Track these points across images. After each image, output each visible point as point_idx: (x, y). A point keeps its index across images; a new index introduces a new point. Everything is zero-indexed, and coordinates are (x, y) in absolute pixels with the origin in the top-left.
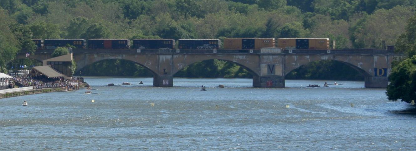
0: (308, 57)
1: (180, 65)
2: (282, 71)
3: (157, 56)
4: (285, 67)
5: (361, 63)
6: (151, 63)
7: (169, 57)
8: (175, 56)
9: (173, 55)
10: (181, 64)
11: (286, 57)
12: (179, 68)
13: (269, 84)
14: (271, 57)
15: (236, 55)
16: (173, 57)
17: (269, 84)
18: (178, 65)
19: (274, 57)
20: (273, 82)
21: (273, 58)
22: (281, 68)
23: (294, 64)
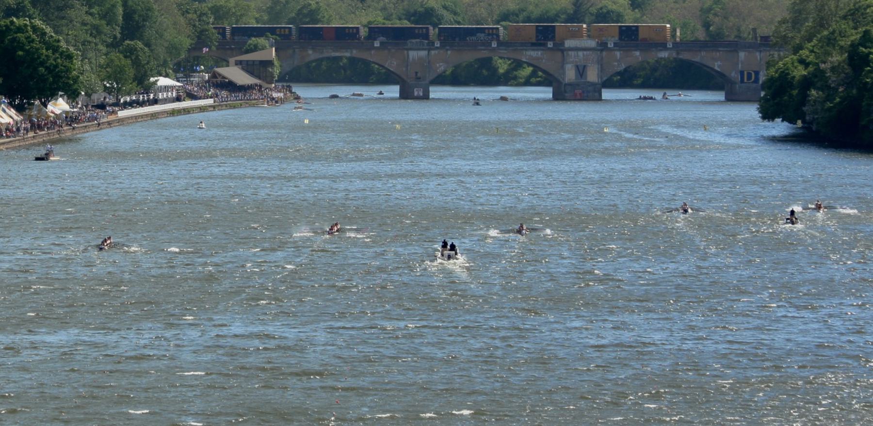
0: (638, 53)
1: (440, 66)
2: (598, 74)
3: (406, 52)
4: (602, 70)
5: (719, 63)
6: (395, 63)
8: (433, 52)
11: (604, 53)
13: (578, 94)
14: (580, 53)
15: (526, 50)
17: (578, 94)
19: (585, 53)
20: (583, 92)
21: (583, 54)
22: (596, 70)
23: (616, 63)
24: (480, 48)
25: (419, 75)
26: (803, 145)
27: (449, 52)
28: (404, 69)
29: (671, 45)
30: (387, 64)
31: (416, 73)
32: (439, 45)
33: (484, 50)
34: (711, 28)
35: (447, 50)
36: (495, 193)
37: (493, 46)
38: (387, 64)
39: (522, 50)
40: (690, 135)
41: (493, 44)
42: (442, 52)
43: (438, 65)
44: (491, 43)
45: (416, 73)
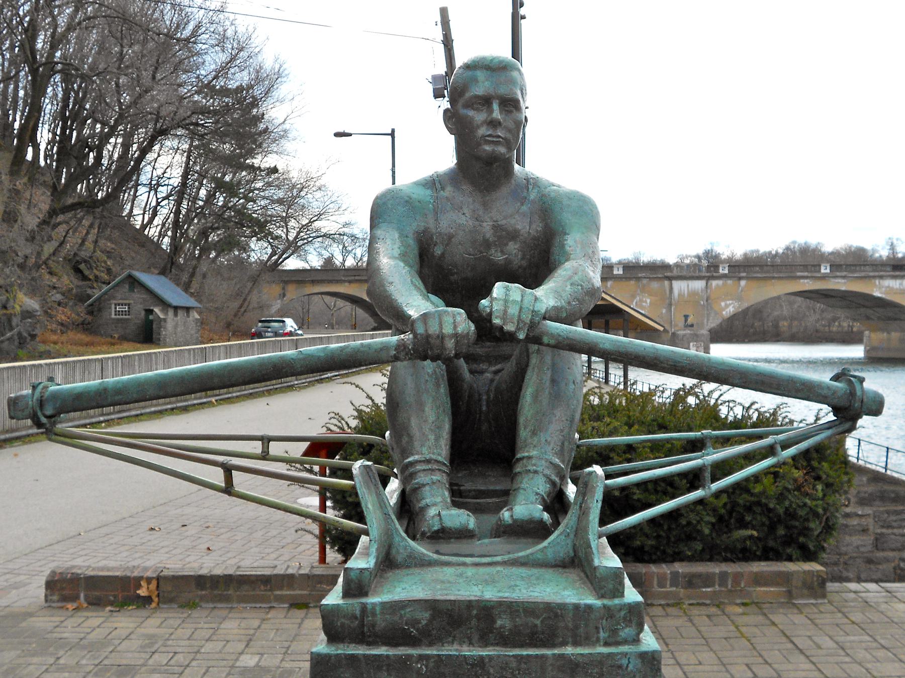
1: (727, 306)
3: (666, 283)
6: (648, 301)
7: (699, 285)
8: (714, 283)
9: (709, 279)
10: (731, 302)
12: (724, 313)
15: (881, 277)
16: (709, 284)
18: (723, 304)
24: (799, 274)
25: (690, 320)
26: (120, 385)
27: (743, 283)
28: (664, 311)
29: (727, 269)
30: (634, 303)
31: (686, 317)
32: (726, 271)
33: (806, 277)
34: (685, 481)
35: (740, 279)
36: (662, 603)
37: (823, 271)
38: (634, 303)
39: (874, 277)
40: (184, 212)
41: (721, 269)
42: (730, 282)
43: (723, 304)
44: (820, 266)
45: (686, 317)
